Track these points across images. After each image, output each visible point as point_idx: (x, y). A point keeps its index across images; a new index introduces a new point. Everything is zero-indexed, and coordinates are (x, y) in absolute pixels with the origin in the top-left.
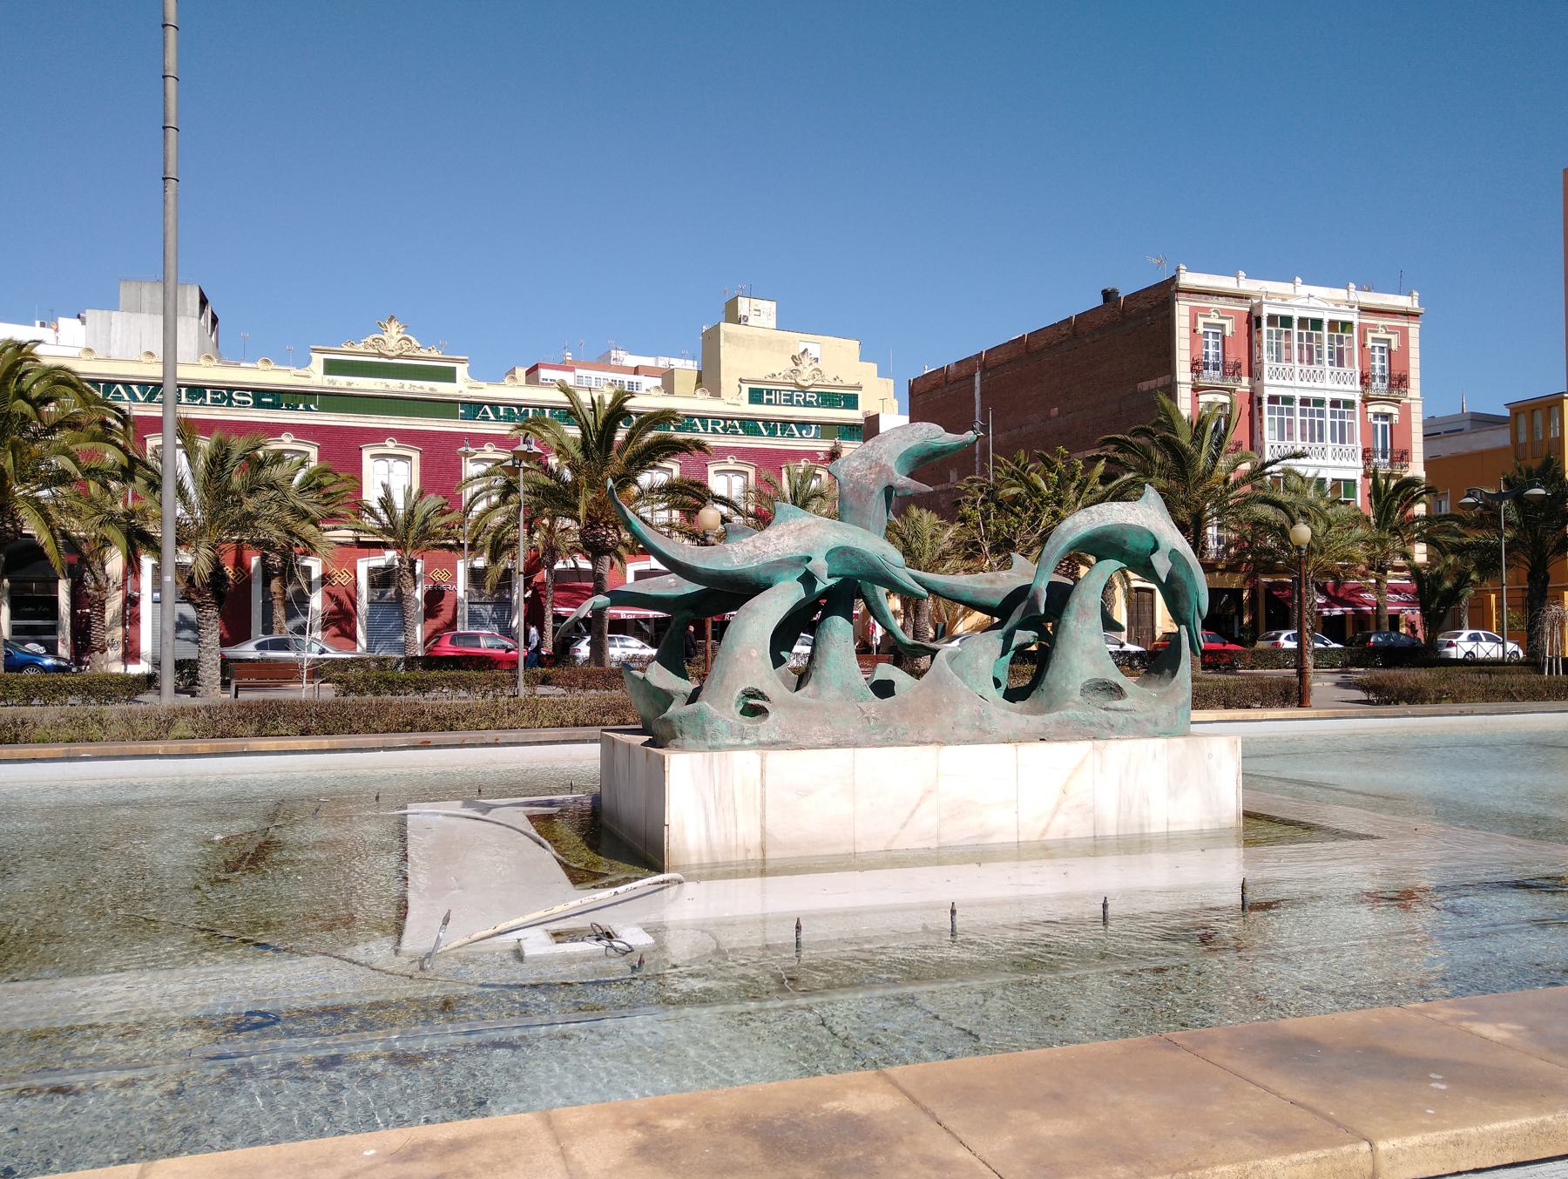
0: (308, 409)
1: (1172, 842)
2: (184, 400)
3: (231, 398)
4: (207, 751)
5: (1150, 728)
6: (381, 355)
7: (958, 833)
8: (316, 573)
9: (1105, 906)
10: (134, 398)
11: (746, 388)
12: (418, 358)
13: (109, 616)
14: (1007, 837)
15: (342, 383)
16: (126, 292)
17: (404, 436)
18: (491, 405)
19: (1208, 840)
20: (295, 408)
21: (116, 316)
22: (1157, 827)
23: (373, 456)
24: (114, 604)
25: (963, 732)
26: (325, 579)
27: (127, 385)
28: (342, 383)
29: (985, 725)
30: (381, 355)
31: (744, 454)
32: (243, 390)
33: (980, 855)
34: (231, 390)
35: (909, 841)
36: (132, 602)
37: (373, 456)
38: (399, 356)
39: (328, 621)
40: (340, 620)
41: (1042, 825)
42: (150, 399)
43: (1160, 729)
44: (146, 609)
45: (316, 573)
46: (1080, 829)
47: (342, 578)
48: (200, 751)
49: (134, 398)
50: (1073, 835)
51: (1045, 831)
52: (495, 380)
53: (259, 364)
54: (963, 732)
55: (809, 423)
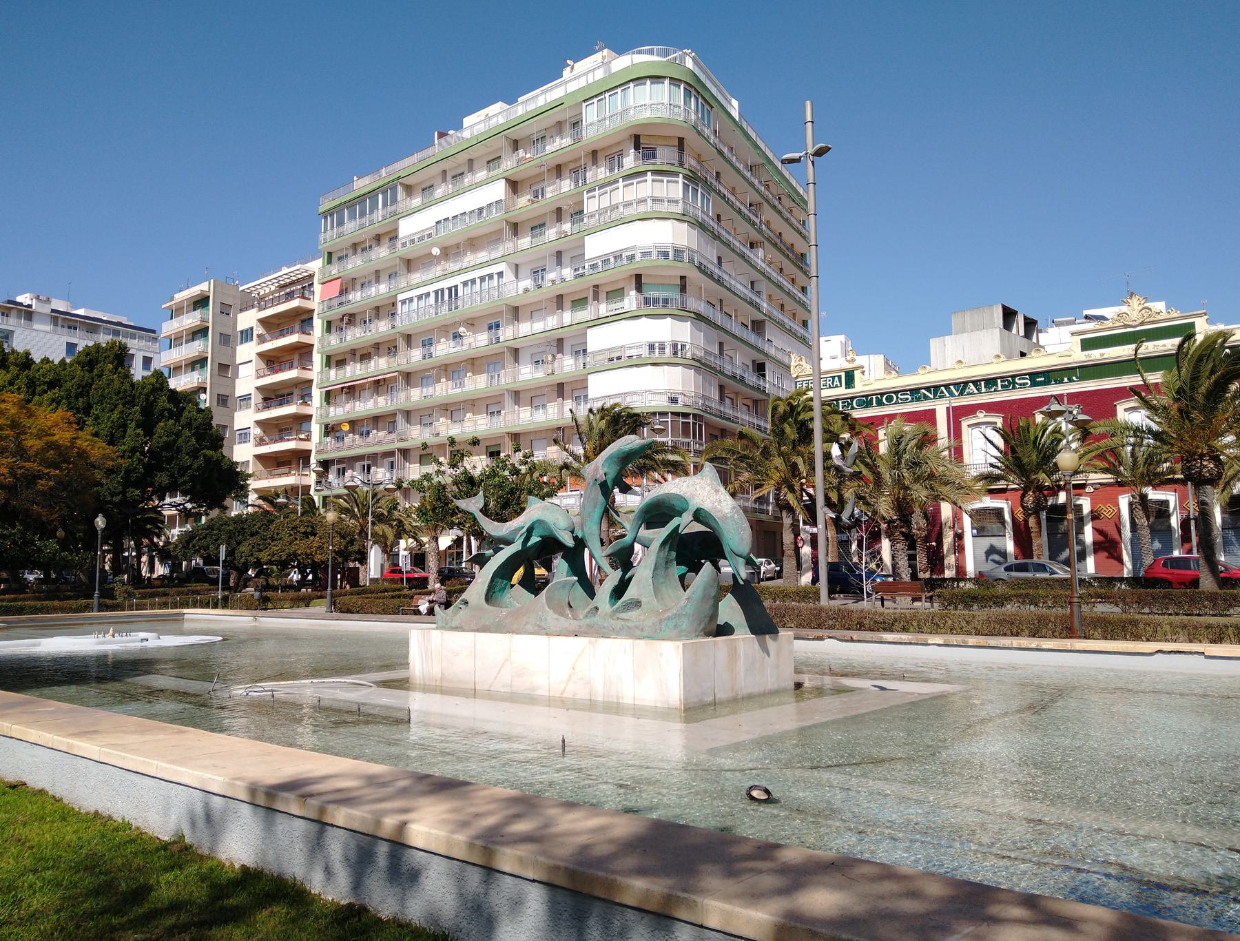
0: (1070, 380)
1: (638, 712)
2: (983, 390)
3: (1014, 383)
4: (1051, 647)
5: (638, 633)
6: (1126, 326)
7: (521, 685)
8: (1086, 509)
9: (563, 741)
10: (952, 394)
11: (1078, 339)
12: (1153, 322)
13: (945, 548)
14: (543, 692)
15: (1096, 355)
16: (956, 321)
17: (990, 408)
18: (973, 382)
19: (663, 714)
20: (1061, 382)
21: (948, 339)
22: (628, 700)
23: (1126, 410)
24: (948, 540)
25: (529, 627)
26: (1095, 516)
27: (947, 386)
28: (1096, 355)
29: (543, 624)
30: (1126, 326)
31: (990, 408)
32: (1022, 376)
33: (529, 699)
34: (1013, 377)
35: (497, 687)
36: (959, 537)
37: (1126, 410)
38: (1142, 324)
39: (1098, 547)
40: (1107, 546)
41: (563, 686)
42: (961, 394)
43: (645, 634)
44: (968, 540)
45: (1086, 509)
46: (583, 694)
47: (1107, 511)
48: (1044, 647)
49: (952, 394)
50: (578, 697)
51: (563, 692)
52: (912, 371)
53: (920, 371)
54: (529, 627)
55: (996, 378)
